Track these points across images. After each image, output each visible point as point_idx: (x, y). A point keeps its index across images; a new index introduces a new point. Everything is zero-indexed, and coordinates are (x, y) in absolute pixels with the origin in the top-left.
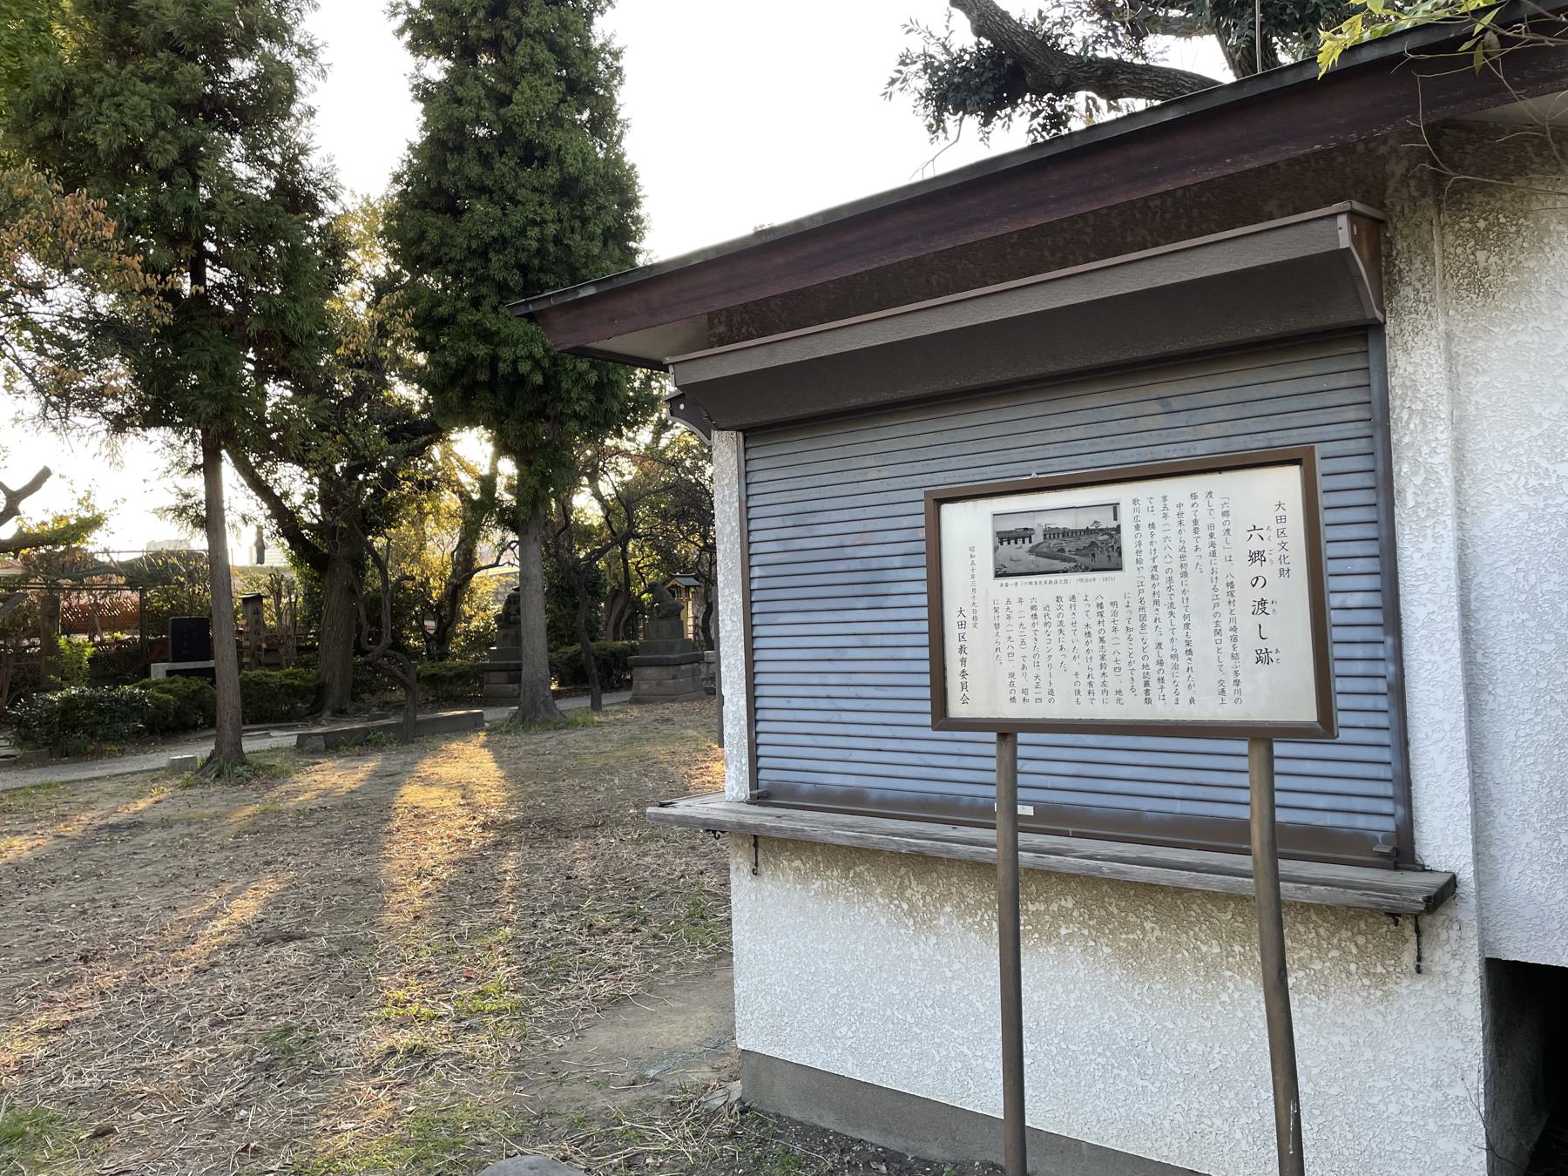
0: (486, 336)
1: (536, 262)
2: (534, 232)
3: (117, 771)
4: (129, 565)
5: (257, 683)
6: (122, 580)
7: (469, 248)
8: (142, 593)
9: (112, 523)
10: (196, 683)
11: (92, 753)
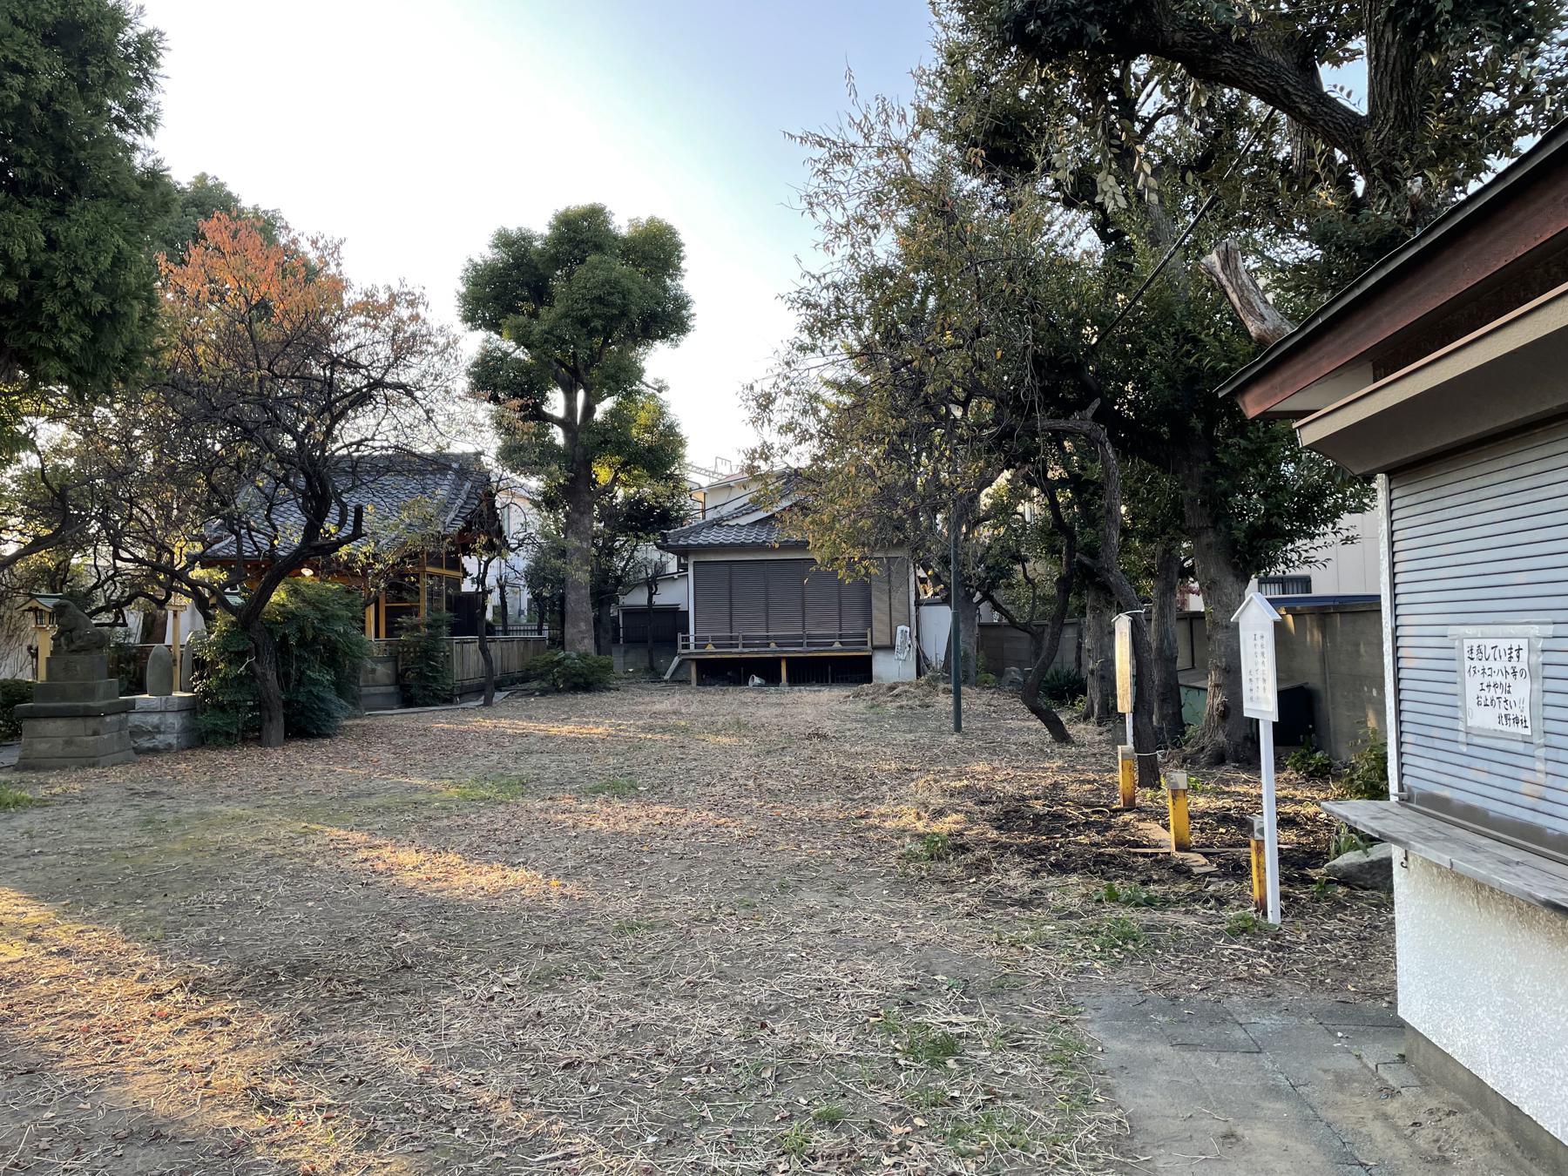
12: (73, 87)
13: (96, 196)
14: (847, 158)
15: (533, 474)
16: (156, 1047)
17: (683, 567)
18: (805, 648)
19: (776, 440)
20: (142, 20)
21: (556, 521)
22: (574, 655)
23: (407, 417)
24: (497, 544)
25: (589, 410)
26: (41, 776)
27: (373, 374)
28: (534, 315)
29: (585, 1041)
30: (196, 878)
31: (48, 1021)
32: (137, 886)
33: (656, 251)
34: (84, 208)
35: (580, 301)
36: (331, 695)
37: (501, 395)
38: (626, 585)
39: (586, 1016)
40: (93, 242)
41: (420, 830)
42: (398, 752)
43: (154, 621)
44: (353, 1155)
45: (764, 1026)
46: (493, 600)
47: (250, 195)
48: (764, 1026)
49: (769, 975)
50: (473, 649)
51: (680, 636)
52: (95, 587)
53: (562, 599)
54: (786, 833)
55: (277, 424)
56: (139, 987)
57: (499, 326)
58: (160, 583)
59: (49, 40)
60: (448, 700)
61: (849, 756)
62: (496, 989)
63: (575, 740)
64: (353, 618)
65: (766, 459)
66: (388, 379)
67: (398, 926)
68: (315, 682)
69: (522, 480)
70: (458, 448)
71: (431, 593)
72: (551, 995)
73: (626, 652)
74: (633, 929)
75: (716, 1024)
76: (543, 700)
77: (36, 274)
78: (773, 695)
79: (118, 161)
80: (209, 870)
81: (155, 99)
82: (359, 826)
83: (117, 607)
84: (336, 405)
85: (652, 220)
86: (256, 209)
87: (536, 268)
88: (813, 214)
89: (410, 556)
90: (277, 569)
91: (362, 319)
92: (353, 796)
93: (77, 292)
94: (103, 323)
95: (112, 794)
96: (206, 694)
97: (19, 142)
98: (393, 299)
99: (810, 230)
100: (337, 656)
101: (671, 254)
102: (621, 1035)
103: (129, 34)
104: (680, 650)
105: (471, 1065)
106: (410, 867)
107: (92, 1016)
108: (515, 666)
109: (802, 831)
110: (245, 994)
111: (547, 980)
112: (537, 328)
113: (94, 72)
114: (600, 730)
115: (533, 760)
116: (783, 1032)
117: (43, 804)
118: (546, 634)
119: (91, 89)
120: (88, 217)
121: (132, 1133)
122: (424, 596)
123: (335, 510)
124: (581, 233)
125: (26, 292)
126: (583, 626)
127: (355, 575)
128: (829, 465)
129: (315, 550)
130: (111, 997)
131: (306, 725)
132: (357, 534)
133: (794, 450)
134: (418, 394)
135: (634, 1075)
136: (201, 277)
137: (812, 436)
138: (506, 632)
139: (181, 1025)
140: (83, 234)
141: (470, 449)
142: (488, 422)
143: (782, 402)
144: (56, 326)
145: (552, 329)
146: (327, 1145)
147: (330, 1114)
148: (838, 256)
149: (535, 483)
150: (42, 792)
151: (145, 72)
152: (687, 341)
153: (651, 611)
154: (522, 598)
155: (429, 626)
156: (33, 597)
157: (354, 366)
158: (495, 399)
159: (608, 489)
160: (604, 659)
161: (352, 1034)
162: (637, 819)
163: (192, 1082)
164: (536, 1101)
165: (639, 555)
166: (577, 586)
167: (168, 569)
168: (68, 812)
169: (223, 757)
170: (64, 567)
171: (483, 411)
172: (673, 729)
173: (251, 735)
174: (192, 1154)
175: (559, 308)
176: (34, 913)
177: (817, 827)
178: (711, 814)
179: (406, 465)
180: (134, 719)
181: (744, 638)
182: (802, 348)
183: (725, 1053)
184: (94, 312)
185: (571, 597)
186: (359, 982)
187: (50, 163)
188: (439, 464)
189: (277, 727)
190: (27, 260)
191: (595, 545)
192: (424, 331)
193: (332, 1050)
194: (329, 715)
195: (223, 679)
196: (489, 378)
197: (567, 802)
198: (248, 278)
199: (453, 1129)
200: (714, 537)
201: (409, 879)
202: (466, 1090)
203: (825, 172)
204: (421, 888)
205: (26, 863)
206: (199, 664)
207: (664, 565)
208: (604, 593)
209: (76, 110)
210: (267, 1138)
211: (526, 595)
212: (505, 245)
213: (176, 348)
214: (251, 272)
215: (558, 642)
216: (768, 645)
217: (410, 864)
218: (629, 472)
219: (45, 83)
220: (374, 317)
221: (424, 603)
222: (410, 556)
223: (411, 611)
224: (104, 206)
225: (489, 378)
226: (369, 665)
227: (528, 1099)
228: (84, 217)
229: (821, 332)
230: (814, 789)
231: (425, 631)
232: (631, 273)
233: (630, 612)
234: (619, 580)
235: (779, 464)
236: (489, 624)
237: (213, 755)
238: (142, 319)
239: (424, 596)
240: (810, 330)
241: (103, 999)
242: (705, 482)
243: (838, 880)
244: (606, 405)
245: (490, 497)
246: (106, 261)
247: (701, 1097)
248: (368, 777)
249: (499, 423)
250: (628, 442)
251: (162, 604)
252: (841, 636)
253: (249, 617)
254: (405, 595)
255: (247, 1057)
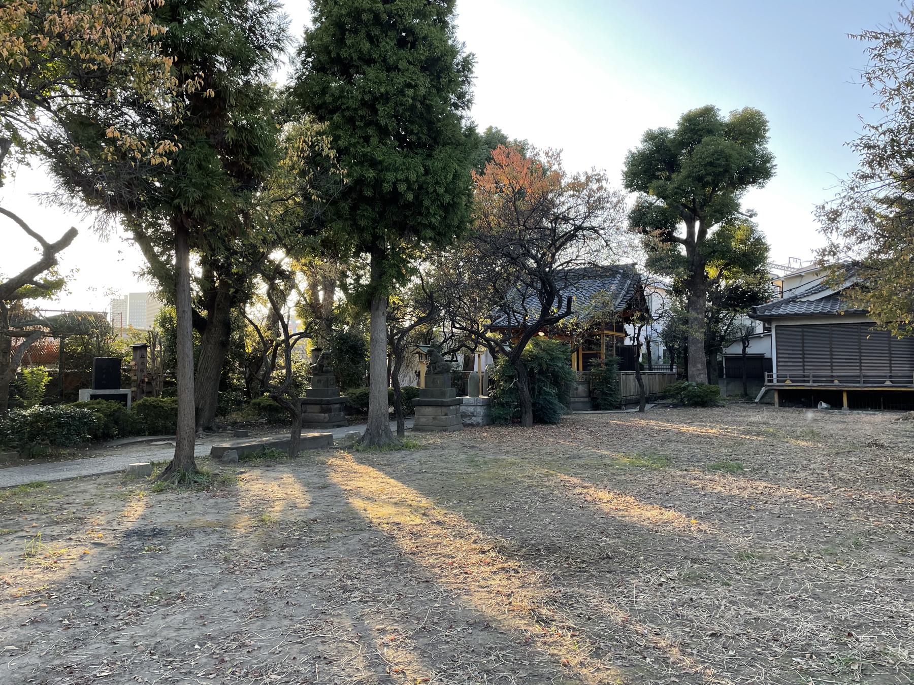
0: (374, 164)
1: (408, 114)
2: (410, 92)
3: (84, 473)
4: (54, 320)
5: (155, 407)
6: (47, 330)
7: (363, 99)
8: (63, 338)
9: (69, 285)
10: (115, 405)
11: (51, 455)
12: (434, 91)
13: (444, 145)
14: (898, 43)
15: (667, 274)
16: (484, 579)
17: (767, 330)
18: (861, 384)
19: (841, 241)
20: (464, 50)
21: (681, 302)
22: (694, 384)
23: (594, 245)
24: (646, 318)
25: (703, 232)
26: (424, 434)
27: (577, 222)
28: (668, 179)
29: (723, 622)
30: (496, 493)
31: (434, 557)
32: (469, 493)
33: (750, 128)
34: (440, 152)
35: (701, 167)
36: (556, 402)
37: (648, 229)
38: (727, 341)
39: (724, 606)
40: (444, 168)
41: (609, 480)
42: (592, 434)
43: (469, 359)
44: (589, 660)
45: (850, 635)
46: (643, 350)
47: (512, 134)
48: (850, 635)
49: (851, 602)
50: (632, 378)
51: (766, 374)
52: (444, 342)
53: (686, 350)
54: (857, 509)
55: (528, 254)
56: (474, 546)
57: (647, 188)
58: (473, 340)
59: (423, 69)
60: (618, 408)
61: (903, 461)
62: (663, 580)
63: (698, 436)
64: (566, 359)
65: (834, 254)
66: (585, 225)
67: (602, 533)
68: (548, 394)
69: (660, 278)
70: (624, 261)
71: (607, 346)
72: (698, 589)
73: (728, 383)
74: (749, 558)
75: (814, 628)
76: (675, 410)
77: (420, 187)
78: (836, 415)
79: (454, 125)
80: (501, 489)
81: (471, 90)
82: (575, 475)
83: (453, 352)
84: (558, 242)
85: (746, 109)
86: (515, 141)
87: (670, 150)
88: (871, 85)
89: (596, 325)
90: (527, 332)
91: (572, 193)
92: (570, 457)
93: (438, 195)
94: (449, 208)
95: (454, 445)
96: (495, 397)
97: (412, 122)
98: (588, 179)
99: (872, 95)
100: (558, 379)
101: (759, 129)
102: (747, 623)
103: (459, 58)
104: (766, 383)
105: (652, 622)
106: (605, 500)
107: (453, 557)
108: (657, 389)
109: (870, 510)
110: (524, 558)
111: (693, 579)
112: (670, 186)
113: (443, 81)
114: (713, 431)
115: (673, 445)
116: (865, 642)
117: (425, 448)
118: (675, 371)
119: (442, 90)
120: (442, 156)
121: (475, 622)
122: (603, 347)
123: (556, 300)
124: (699, 125)
125: (416, 197)
126: (699, 366)
127: (567, 335)
128: (883, 256)
129: (547, 322)
130: (461, 550)
131: (543, 417)
132: (569, 312)
133: (856, 248)
134: (601, 232)
135: (759, 650)
136: (492, 180)
137: (870, 237)
138: (650, 369)
139: (495, 569)
140: (440, 165)
141: (630, 261)
142: (640, 245)
143: (847, 215)
144: (429, 212)
145: (680, 186)
146: (574, 651)
147: (575, 633)
148: (892, 110)
149: (668, 280)
150: (424, 442)
151: (466, 77)
152: (771, 183)
153: (744, 358)
154: (660, 350)
155: (607, 364)
156: (418, 347)
157: (566, 219)
158: (645, 232)
159: (716, 281)
160: (713, 387)
161: (582, 590)
162: (745, 488)
163: (502, 600)
164: (695, 652)
165: (736, 322)
166: (696, 341)
167: (477, 333)
168: (436, 453)
169: (504, 431)
170: (430, 332)
171: (637, 239)
172: (766, 434)
173: (516, 420)
174: (505, 640)
175: (684, 172)
176: (425, 502)
177: (882, 507)
178: (798, 491)
179: (594, 273)
180: (463, 408)
181: (814, 376)
182: (864, 177)
183: (823, 648)
184: (445, 204)
185: (692, 349)
186: (583, 562)
187: (425, 131)
188: (612, 271)
189: (529, 417)
190: (417, 181)
191: (707, 316)
192: (605, 195)
193: (572, 597)
194: (555, 412)
195: (503, 390)
196: (641, 219)
197: (697, 473)
198: (515, 178)
199: (645, 658)
200: (790, 309)
201: (606, 508)
202: (650, 636)
203: (880, 55)
204: (613, 514)
205: (420, 476)
206: (491, 382)
207: (753, 329)
208: (713, 346)
209: (437, 102)
210: (542, 639)
211: (662, 348)
212: (651, 139)
213: (481, 218)
214: (515, 174)
215: (684, 376)
216: (832, 381)
217: (605, 499)
218: (730, 270)
219: (422, 91)
220: (578, 191)
221: (603, 351)
222: (596, 325)
223: (597, 356)
224: (448, 149)
225: (641, 219)
226: (575, 385)
227: (689, 650)
228: (441, 154)
229: (880, 164)
230: (875, 481)
231: (604, 367)
232: (732, 145)
233: (731, 359)
234: (723, 338)
235: (845, 257)
236: (641, 364)
237: (499, 429)
238: (466, 205)
239: (603, 347)
240: (870, 164)
241: (458, 549)
242: (781, 274)
243: (900, 545)
244: (715, 228)
245: (640, 290)
246: (450, 177)
247: (806, 673)
248: (578, 448)
249: (647, 245)
250: (729, 250)
251: (473, 351)
252: (891, 377)
253: (515, 357)
254: (593, 346)
255: (529, 592)
